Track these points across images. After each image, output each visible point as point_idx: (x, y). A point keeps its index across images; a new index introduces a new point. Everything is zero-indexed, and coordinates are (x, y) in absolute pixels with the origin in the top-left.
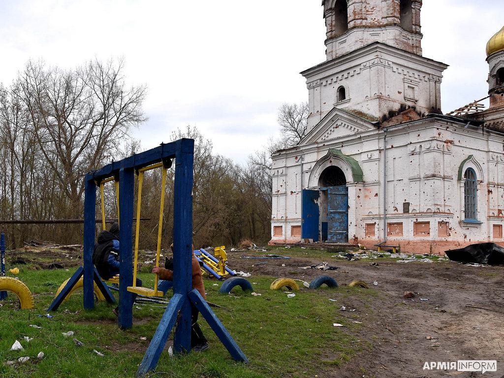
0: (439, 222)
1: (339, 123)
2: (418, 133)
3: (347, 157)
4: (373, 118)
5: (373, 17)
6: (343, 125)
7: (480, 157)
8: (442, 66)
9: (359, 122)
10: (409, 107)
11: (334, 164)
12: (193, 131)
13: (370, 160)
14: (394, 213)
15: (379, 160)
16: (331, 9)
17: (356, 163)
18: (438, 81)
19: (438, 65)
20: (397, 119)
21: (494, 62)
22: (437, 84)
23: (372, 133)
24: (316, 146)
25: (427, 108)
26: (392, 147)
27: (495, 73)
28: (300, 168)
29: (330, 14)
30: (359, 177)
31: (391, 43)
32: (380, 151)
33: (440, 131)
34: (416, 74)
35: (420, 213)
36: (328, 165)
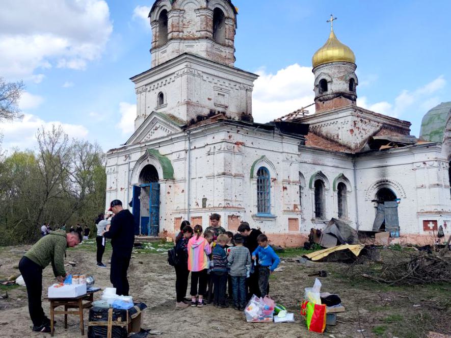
0: (229, 216)
1: (158, 125)
2: (213, 135)
3: (162, 156)
4: (182, 121)
5: (189, 30)
7: (270, 156)
8: (253, 76)
9: (171, 125)
10: (219, 112)
11: (150, 163)
12: (57, 129)
13: (179, 159)
14: (196, 208)
15: (185, 159)
16: (155, 21)
17: (169, 162)
18: (249, 90)
19: (248, 75)
20: (199, 123)
21: (318, 73)
22: (248, 92)
23: (179, 135)
24: (139, 146)
25: (237, 114)
26: (195, 148)
27: (318, 83)
28: (127, 165)
29: (155, 26)
30: (169, 175)
31: (204, 55)
32: (186, 151)
33: (230, 134)
34: (227, 83)
35: (214, 207)
36: (146, 163)
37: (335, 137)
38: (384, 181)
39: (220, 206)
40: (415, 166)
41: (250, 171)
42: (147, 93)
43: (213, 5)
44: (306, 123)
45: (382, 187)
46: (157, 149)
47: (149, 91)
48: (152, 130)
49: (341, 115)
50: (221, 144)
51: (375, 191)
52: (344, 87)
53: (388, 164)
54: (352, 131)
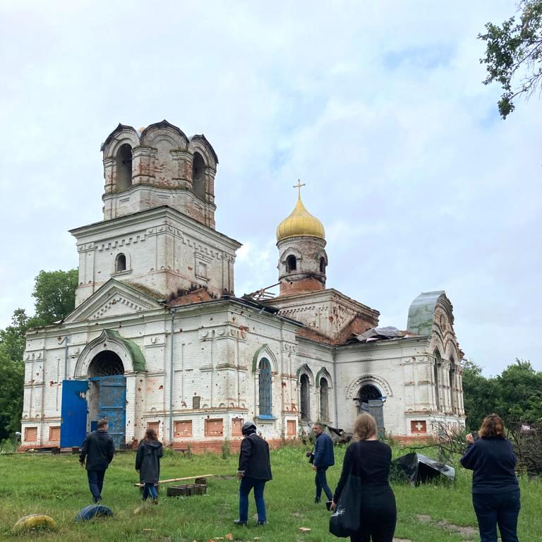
1: (117, 298)
2: (211, 316)
4: (158, 295)
6: (122, 301)
8: (236, 244)
13: (155, 345)
15: (165, 345)
16: (112, 157)
18: (231, 261)
23: (158, 313)
24: (86, 324)
26: (181, 331)
29: (111, 163)
32: (167, 335)
36: (101, 349)
37: (312, 325)
38: (368, 377)
39: (222, 406)
40: (403, 361)
41: (252, 363)
42: (98, 253)
43: (194, 149)
44: (275, 306)
45: (365, 384)
46: (116, 330)
47: (101, 251)
48: (108, 304)
49: (318, 299)
50: (224, 327)
51: (358, 388)
52: (313, 266)
53: (373, 358)
54: (331, 319)
